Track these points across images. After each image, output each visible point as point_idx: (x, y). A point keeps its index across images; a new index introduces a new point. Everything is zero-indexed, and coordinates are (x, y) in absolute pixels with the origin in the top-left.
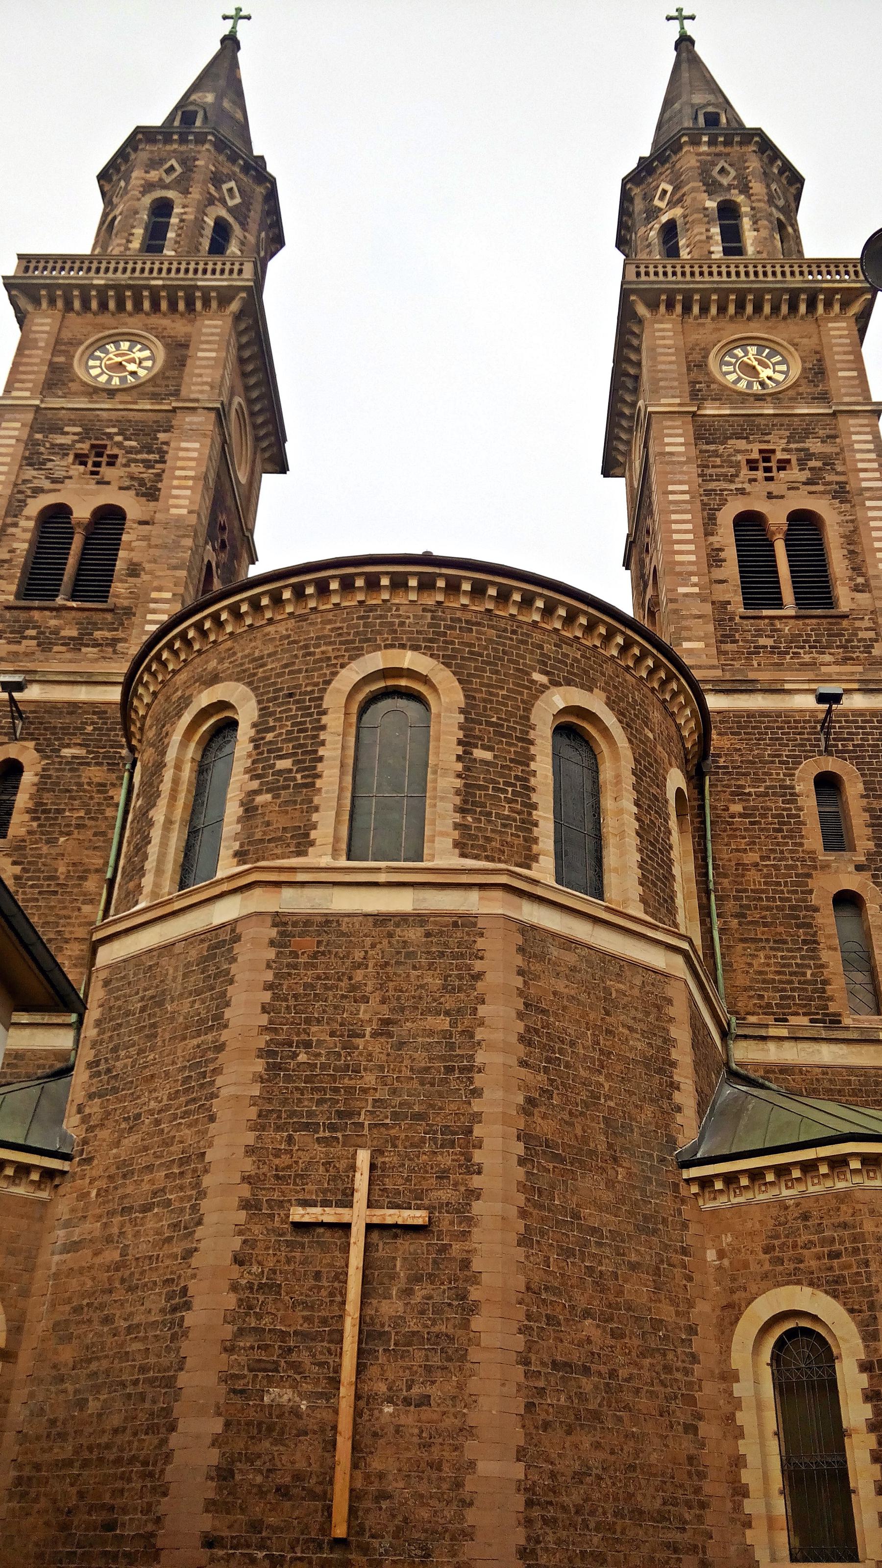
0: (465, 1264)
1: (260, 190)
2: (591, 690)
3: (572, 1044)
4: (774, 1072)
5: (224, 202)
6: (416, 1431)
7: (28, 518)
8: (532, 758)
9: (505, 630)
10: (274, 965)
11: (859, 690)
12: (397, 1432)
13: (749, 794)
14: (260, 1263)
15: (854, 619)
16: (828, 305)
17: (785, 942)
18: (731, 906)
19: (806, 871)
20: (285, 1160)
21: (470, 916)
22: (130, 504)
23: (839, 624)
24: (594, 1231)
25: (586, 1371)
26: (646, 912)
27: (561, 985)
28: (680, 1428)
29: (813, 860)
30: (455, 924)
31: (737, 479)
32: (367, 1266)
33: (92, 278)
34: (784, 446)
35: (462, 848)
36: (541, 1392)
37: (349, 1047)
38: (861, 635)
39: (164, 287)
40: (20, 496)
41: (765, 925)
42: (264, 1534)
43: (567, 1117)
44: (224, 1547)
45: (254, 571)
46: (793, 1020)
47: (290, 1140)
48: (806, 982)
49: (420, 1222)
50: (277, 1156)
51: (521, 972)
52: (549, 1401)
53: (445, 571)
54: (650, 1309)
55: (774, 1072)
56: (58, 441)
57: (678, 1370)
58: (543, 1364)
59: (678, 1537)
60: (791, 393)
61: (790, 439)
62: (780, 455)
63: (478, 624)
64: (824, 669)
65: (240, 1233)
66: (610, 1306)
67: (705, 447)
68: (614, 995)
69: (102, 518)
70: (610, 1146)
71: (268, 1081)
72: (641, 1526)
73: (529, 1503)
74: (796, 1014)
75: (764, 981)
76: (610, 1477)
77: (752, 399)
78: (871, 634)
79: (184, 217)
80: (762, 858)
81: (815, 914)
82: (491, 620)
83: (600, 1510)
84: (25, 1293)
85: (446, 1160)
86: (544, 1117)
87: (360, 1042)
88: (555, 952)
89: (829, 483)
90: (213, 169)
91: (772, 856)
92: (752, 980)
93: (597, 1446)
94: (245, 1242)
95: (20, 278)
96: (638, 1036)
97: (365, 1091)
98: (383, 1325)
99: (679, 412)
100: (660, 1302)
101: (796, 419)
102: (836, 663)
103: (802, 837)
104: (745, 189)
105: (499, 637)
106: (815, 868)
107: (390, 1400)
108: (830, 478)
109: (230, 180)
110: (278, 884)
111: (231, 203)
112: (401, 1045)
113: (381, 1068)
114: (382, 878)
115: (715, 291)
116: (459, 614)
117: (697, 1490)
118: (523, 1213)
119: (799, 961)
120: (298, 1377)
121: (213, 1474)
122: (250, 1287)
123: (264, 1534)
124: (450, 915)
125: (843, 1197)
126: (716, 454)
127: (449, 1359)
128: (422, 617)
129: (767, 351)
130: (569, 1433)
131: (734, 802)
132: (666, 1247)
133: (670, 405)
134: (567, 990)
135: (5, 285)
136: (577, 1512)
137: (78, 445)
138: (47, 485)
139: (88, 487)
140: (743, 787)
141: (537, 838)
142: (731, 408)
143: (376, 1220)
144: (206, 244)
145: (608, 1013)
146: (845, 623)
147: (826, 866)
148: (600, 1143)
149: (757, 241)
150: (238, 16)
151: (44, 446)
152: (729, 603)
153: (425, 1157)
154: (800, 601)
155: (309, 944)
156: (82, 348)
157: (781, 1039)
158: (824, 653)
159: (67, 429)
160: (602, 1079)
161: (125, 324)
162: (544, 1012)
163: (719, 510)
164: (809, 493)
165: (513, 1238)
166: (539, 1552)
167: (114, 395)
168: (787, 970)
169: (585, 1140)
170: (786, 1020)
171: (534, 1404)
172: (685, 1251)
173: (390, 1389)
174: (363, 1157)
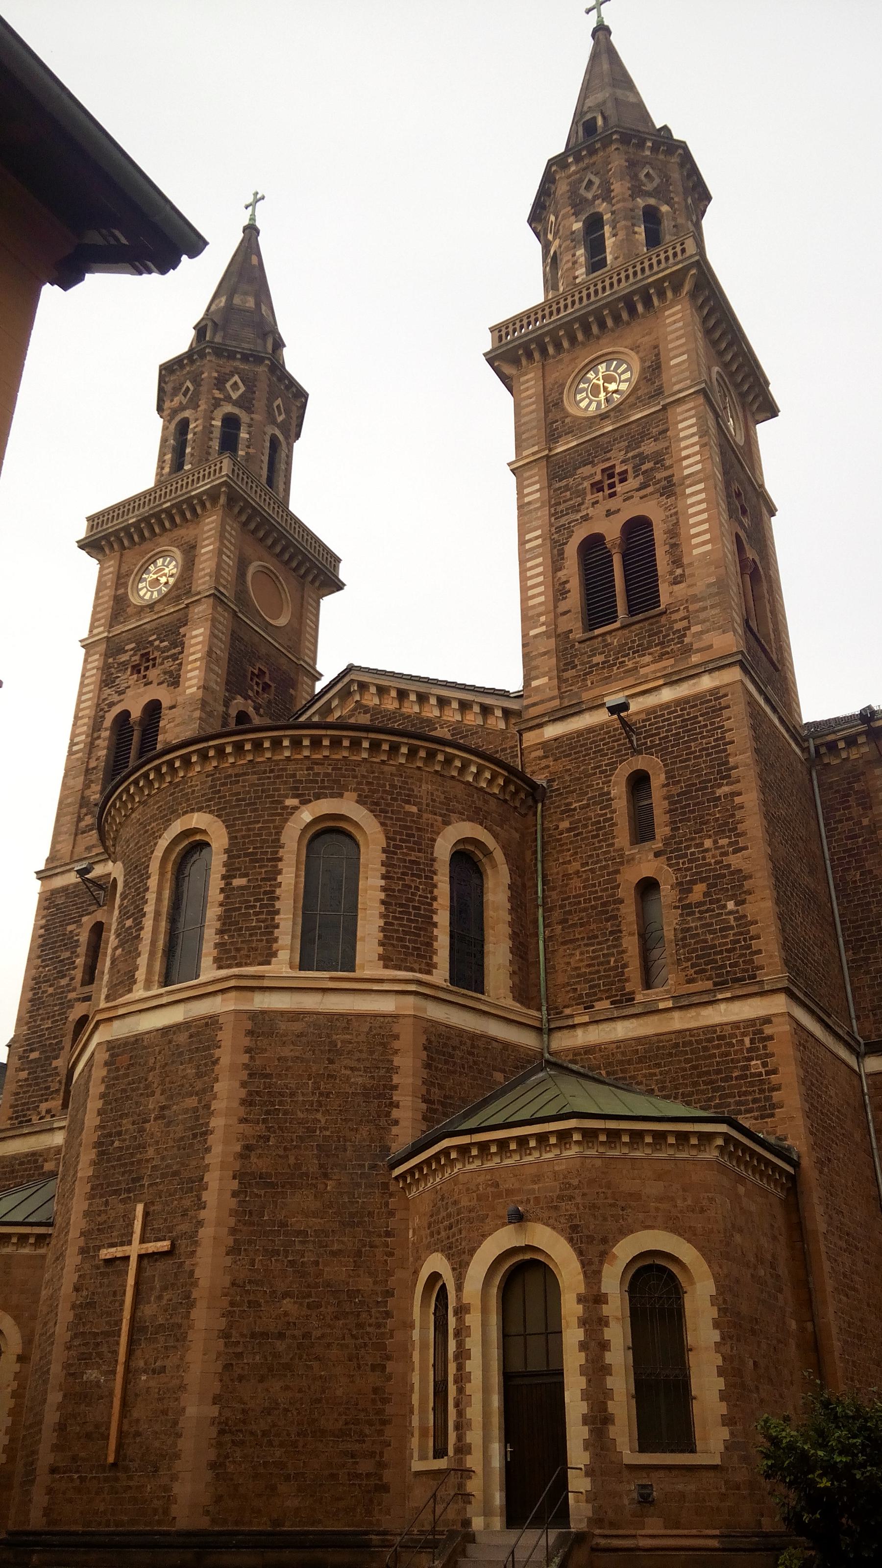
0: (192, 1273)
1: (262, 370)
2: (341, 796)
3: (292, 1095)
4: (580, 1054)
5: (228, 399)
6: (157, 1390)
7: (106, 729)
8: (280, 872)
9: (265, 772)
10: (106, 1080)
11: (664, 684)
12: (147, 1392)
13: (575, 809)
14: (87, 1289)
15: (671, 613)
16: (662, 294)
17: (596, 937)
18: (557, 915)
19: (616, 868)
20: (104, 1217)
21: (211, 1017)
22: (162, 694)
23: (657, 622)
24: (299, 1233)
25: (281, 1336)
27: (286, 1052)
28: (368, 1368)
29: (622, 856)
30: (207, 1024)
31: (583, 507)
32: (137, 1284)
33: (127, 520)
34: (622, 458)
36: (239, 1355)
37: (142, 1130)
38: (677, 626)
39: (172, 506)
40: (101, 713)
41: (582, 925)
42: (78, 1464)
43: (281, 1153)
44: (59, 1473)
45: (319, 686)
46: (598, 1006)
47: (107, 1203)
48: (610, 969)
49: (166, 1249)
50: (99, 1215)
51: (248, 1050)
52: (245, 1361)
53: (211, 743)
54: (348, 1283)
55: (580, 1054)
56: (122, 660)
57: (370, 1325)
58: (242, 1335)
59: (357, 1446)
60: (632, 399)
61: (628, 449)
62: (618, 470)
63: (244, 774)
64: (642, 671)
65: (79, 1270)
66: (309, 1286)
67: (558, 485)
68: (339, 1045)
69: (122, 726)
70: (321, 1166)
71: (98, 1164)
72: (322, 1441)
73: (221, 1432)
74: (601, 999)
75: (579, 976)
76: (296, 1409)
77: (598, 420)
78: (685, 623)
79: (196, 430)
80: (583, 865)
81: (620, 906)
82: (254, 767)
83: (285, 1433)
84: (33, 1318)
85: (187, 1203)
86: (260, 1156)
87: (147, 1125)
88: (283, 1026)
89: (659, 481)
90: (216, 375)
91: (590, 861)
92: (572, 977)
93: (287, 1388)
94: (80, 1276)
95: (92, 535)
96: (361, 1073)
97: (147, 1161)
98: (145, 1322)
99: (535, 460)
100: (359, 1276)
101: (633, 426)
102: (653, 662)
103: (613, 838)
104: (606, 195)
105: (259, 779)
106: (622, 863)
107: (145, 1372)
108: (659, 476)
109: (233, 376)
110: (110, 1019)
111: (235, 396)
112: (168, 1124)
113: (157, 1143)
114: (164, 1000)
115: (560, 327)
116: (230, 771)
117: (380, 1412)
118: (233, 1231)
119: (605, 952)
120: (101, 1361)
121: (57, 1427)
122: (81, 1305)
123: (78, 1464)
124: (204, 1018)
125: (455, 1180)
126: (567, 488)
127: (178, 1340)
128: (206, 782)
129: (615, 363)
130: (261, 1381)
131: (562, 820)
132: (370, 1233)
133: (534, 454)
134: (292, 1053)
135: (80, 547)
136: (263, 1435)
137: (133, 659)
138: (116, 698)
139: (139, 691)
140: (571, 804)
142: (577, 439)
143: (143, 1252)
144: (216, 445)
145: (331, 1061)
146: (663, 619)
147: (631, 859)
148: (312, 1167)
149: (617, 246)
150: (258, 199)
151: (113, 667)
152: (571, 631)
153: (176, 1202)
154: (632, 610)
156: (133, 576)
157: (585, 1024)
158: (644, 655)
159: (127, 648)
160: (319, 1116)
161: (158, 545)
162: (267, 1076)
163: (566, 544)
164: (641, 498)
165: (223, 1250)
166: (228, 1464)
167: (153, 607)
168: (595, 961)
169: (298, 1166)
170: (593, 1007)
171: (232, 1364)
172: (388, 1234)
173: (146, 1364)
174: (140, 1208)
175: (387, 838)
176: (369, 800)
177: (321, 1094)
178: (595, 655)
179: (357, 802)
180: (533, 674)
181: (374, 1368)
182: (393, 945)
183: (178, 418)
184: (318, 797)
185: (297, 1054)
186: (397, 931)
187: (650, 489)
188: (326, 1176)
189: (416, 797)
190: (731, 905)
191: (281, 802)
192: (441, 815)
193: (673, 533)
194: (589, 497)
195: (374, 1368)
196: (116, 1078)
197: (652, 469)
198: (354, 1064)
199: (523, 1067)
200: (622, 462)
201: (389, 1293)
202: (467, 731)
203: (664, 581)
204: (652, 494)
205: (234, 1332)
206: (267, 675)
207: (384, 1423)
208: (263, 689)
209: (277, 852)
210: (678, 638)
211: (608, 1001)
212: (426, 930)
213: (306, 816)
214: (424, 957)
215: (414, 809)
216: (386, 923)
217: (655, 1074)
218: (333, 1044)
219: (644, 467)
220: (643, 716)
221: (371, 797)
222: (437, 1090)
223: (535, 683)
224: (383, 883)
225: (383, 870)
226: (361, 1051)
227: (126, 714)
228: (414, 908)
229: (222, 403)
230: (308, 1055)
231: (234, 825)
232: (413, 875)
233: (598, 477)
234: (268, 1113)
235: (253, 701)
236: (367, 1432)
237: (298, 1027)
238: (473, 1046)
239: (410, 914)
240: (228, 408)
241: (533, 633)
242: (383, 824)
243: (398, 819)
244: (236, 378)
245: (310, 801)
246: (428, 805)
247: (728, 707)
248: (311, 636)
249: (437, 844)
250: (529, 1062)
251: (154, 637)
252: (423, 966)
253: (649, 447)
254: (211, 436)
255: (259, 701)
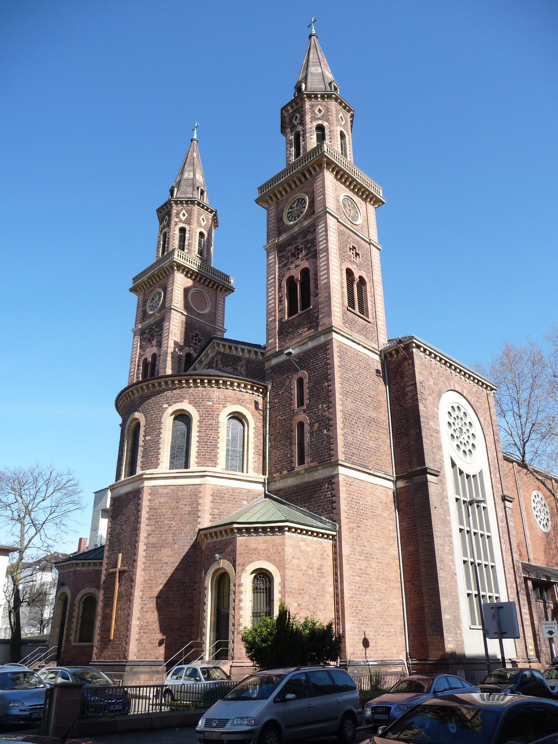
2: (182, 401)
3: (164, 515)
24: (166, 563)
26: (267, 698)
27: (162, 500)
34: (301, 242)
35: (198, 464)
36: (145, 604)
57: (189, 593)
61: (303, 238)
62: (300, 247)
64: (304, 334)
70: (174, 540)
73: (140, 629)
86: (153, 537)
88: (160, 491)
102: (308, 330)
111: (183, 219)
141: (196, 463)
145: (177, 502)
148: (170, 540)
155: (411, 367)
160: (173, 522)
162: (156, 509)
169: (165, 540)
175: (200, 416)
176: (193, 402)
177: (173, 515)
178: (289, 328)
179: (189, 403)
180: (269, 337)
181: (189, 608)
182: (201, 458)
183: (163, 232)
184: (175, 403)
185: (166, 501)
186: (203, 452)
187: (309, 256)
188: (175, 543)
189: (212, 398)
190: (325, 431)
191: (162, 406)
192: (222, 404)
193: (316, 274)
194: (290, 260)
195: (189, 608)
196: (115, 510)
197: (310, 247)
198: (185, 503)
199: (256, 498)
200: (301, 244)
201: (195, 583)
202: (251, 361)
203: (312, 296)
204: (310, 257)
205: (144, 597)
206: (200, 335)
207: (192, 625)
208: (199, 341)
209: (160, 426)
210: (316, 320)
211: (286, 471)
212: (214, 450)
213: (170, 410)
214: (214, 461)
215: (211, 403)
216: (198, 450)
217: (299, 498)
218: (178, 496)
219: (308, 246)
220: (303, 354)
221: (194, 401)
222: (216, 510)
223: (270, 341)
224: (198, 434)
225: (198, 429)
226: (188, 498)
227: (146, 359)
228: (210, 442)
229: (178, 223)
230: (169, 501)
231: (147, 416)
232: (210, 429)
233: (293, 251)
234: (155, 522)
235: (193, 347)
236: (187, 629)
237: (166, 491)
238: (233, 492)
239: (208, 445)
240: (181, 225)
241: (270, 320)
242: (198, 411)
243: (204, 408)
244: (184, 211)
245: (172, 405)
246: (217, 401)
247: (329, 349)
248: (221, 314)
249: (220, 416)
250: (259, 495)
251: (154, 327)
252: (213, 464)
253: (309, 237)
254: (174, 238)
255: (196, 347)
